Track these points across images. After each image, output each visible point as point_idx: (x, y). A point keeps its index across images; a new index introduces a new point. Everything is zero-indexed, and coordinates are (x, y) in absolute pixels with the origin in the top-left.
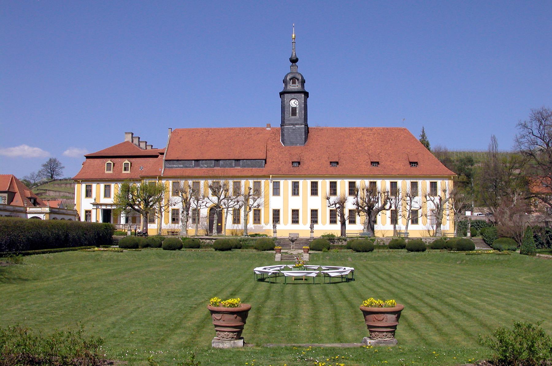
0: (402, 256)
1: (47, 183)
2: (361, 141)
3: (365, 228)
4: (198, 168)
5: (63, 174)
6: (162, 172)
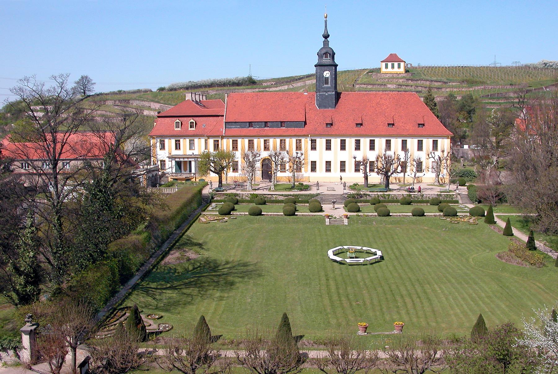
0: (408, 220)
1: (82, 100)
2: (379, 105)
3: (382, 178)
4: (252, 128)
5: (94, 90)
6: (224, 132)
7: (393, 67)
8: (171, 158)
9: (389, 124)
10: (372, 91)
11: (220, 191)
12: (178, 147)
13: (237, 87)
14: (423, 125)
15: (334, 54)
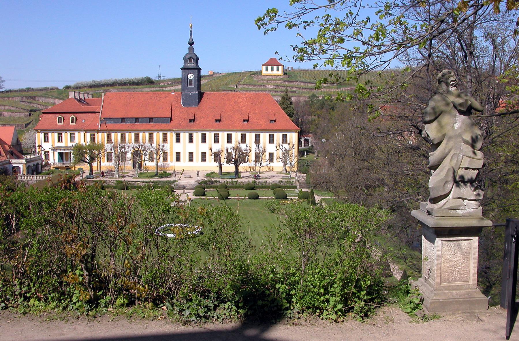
4: (124, 123)
7: (272, 70)
8: (54, 149)
9: (244, 120)
10: (252, 91)
11: (91, 178)
12: (60, 139)
13: (137, 87)
14: (275, 121)
15: (197, 59)
